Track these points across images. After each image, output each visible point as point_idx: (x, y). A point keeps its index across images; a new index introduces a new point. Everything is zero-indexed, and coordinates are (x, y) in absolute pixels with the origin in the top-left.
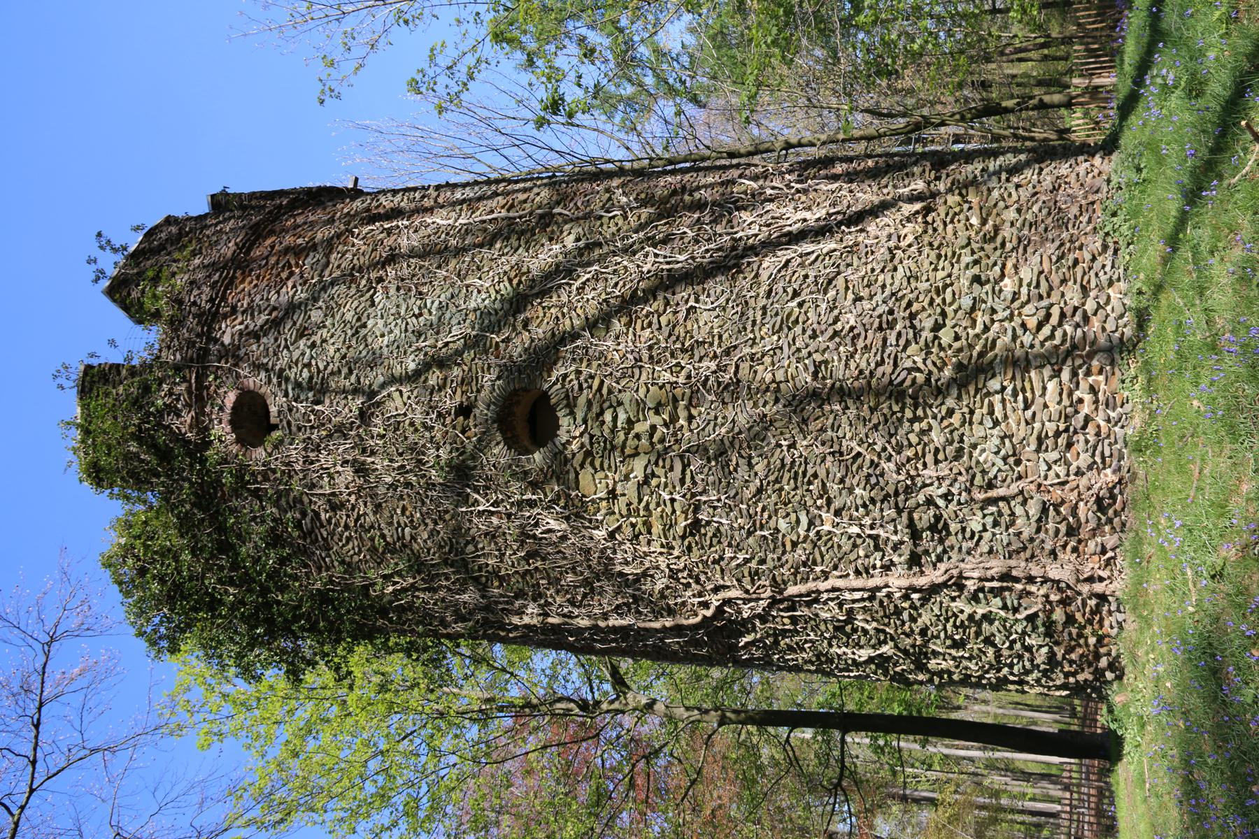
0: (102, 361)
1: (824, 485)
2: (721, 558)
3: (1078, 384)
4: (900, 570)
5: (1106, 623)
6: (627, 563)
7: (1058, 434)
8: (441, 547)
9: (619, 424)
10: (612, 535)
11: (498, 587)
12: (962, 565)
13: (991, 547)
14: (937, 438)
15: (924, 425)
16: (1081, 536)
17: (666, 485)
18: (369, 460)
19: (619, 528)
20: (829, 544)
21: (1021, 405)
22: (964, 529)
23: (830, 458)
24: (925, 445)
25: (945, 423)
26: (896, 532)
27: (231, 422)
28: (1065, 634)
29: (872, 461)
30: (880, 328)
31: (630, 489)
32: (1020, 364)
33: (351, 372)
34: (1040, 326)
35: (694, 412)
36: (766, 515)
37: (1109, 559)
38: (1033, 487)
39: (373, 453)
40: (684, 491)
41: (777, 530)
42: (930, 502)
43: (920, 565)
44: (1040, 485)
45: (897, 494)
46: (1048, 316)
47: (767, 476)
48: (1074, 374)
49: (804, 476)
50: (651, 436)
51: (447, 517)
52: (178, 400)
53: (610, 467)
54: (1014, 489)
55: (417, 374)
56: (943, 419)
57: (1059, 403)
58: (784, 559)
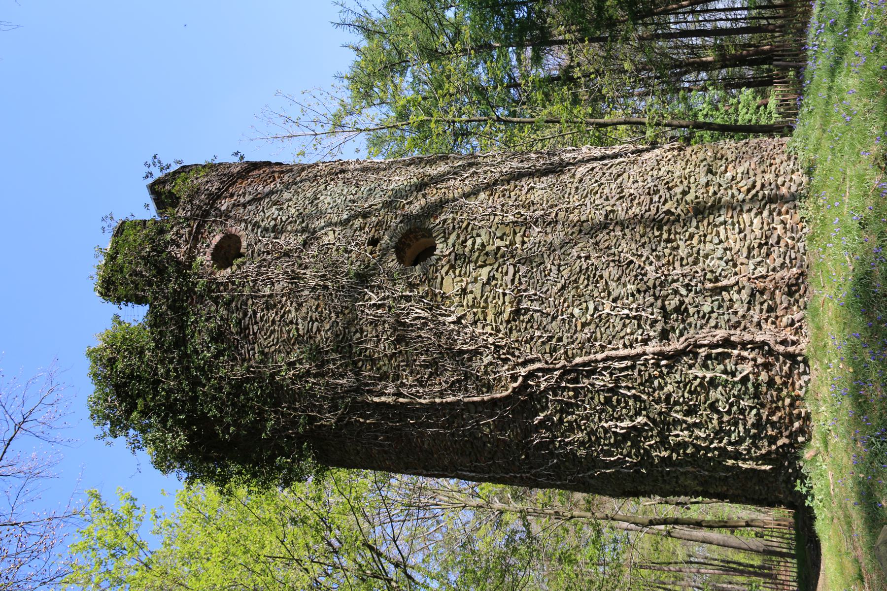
0: (135, 218)
1: (607, 283)
2: (532, 338)
3: (773, 220)
4: (653, 343)
5: (797, 386)
6: (466, 343)
7: (760, 246)
8: (337, 336)
9: (476, 247)
10: (458, 321)
11: (370, 370)
12: (697, 336)
13: (717, 323)
14: (683, 252)
15: (675, 244)
16: (778, 314)
17: (501, 285)
18: (302, 272)
19: (465, 315)
20: (607, 325)
21: (737, 230)
22: (698, 312)
23: (612, 264)
24: (675, 256)
25: (688, 242)
26: (652, 314)
27: (212, 254)
28: (769, 396)
29: (640, 266)
30: (649, 194)
31: (477, 288)
32: (736, 207)
33: (303, 221)
34: (749, 191)
35: (526, 239)
36: (566, 305)
37: (796, 328)
38: (746, 279)
39: (306, 267)
40: (513, 287)
41: (572, 315)
42: (676, 292)
43: (669, 340)
44: (749, 279)
45: (655, 287)
46: (754, 186)
47: (569, 277)
48: (771, 213)
49: (594, 277)
50: (496, 254)
51: (347, 312)
52: (181, 237)
53: (465, 273)
54: (732, 280)
55: (348, 220)
56: (686, 241)
57: (762, 228)
58: (575, 337)
